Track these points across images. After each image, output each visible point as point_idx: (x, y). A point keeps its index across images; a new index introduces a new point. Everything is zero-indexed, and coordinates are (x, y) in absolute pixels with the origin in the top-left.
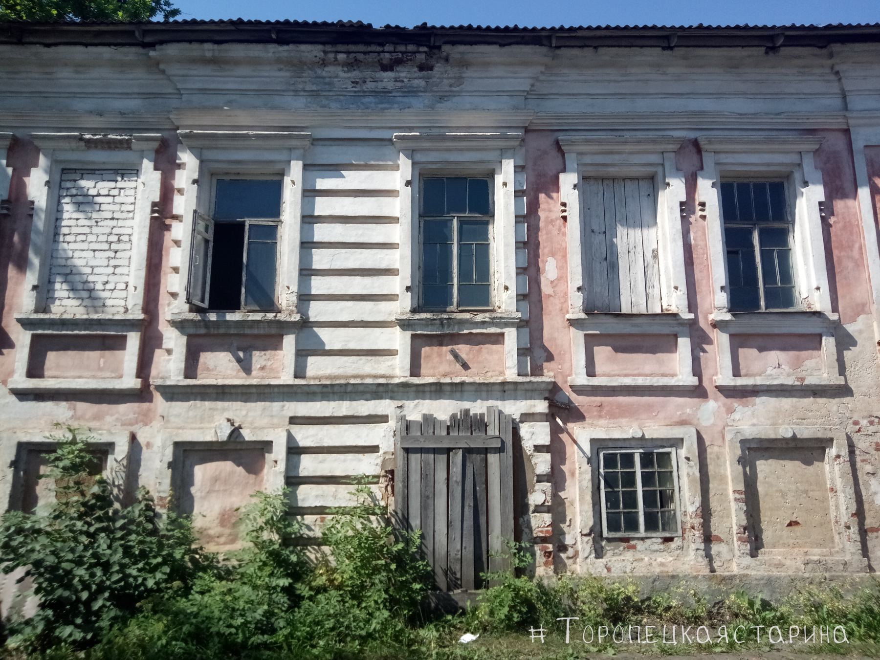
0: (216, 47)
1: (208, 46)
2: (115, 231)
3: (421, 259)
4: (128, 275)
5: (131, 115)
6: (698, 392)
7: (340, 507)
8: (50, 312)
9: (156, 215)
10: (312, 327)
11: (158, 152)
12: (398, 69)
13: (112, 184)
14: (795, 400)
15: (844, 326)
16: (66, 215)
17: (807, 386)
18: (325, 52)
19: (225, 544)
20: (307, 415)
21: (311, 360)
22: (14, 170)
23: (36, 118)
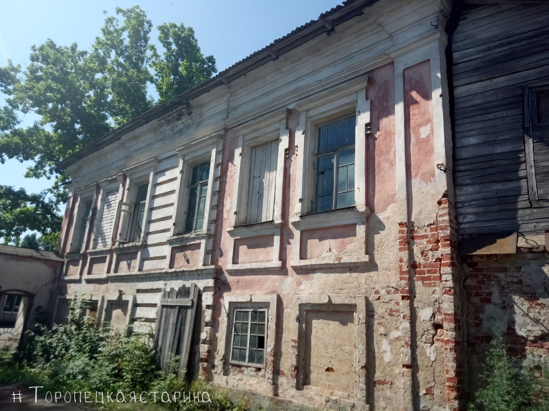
6: (282, 270)
13: (114, 196)
14: (337, 275)
15: (377, 215)
17: (344, 263)
21: (146, 263)
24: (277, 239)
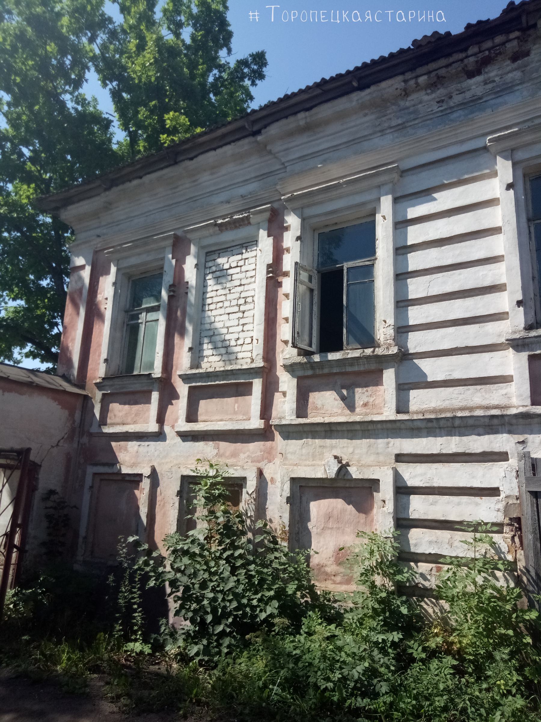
0: (307, 113)
1: (301, 115)
2: (243, 295)
3: (535, 268)
4: (253, 330)
5: (249, 196)
7: (457, 557)
8: (201, 368)
9: (271, 275)
10: (412, 359)
11: (270, 221)
12: (486, 70)
13: (239, 257)
16: (209, 289)
18: (405, 81)
19: (340, 583)
20: (414, 452)
21: (414, 394)
22: (176, 261)
23: (189, 218)
24: (155, 396)
